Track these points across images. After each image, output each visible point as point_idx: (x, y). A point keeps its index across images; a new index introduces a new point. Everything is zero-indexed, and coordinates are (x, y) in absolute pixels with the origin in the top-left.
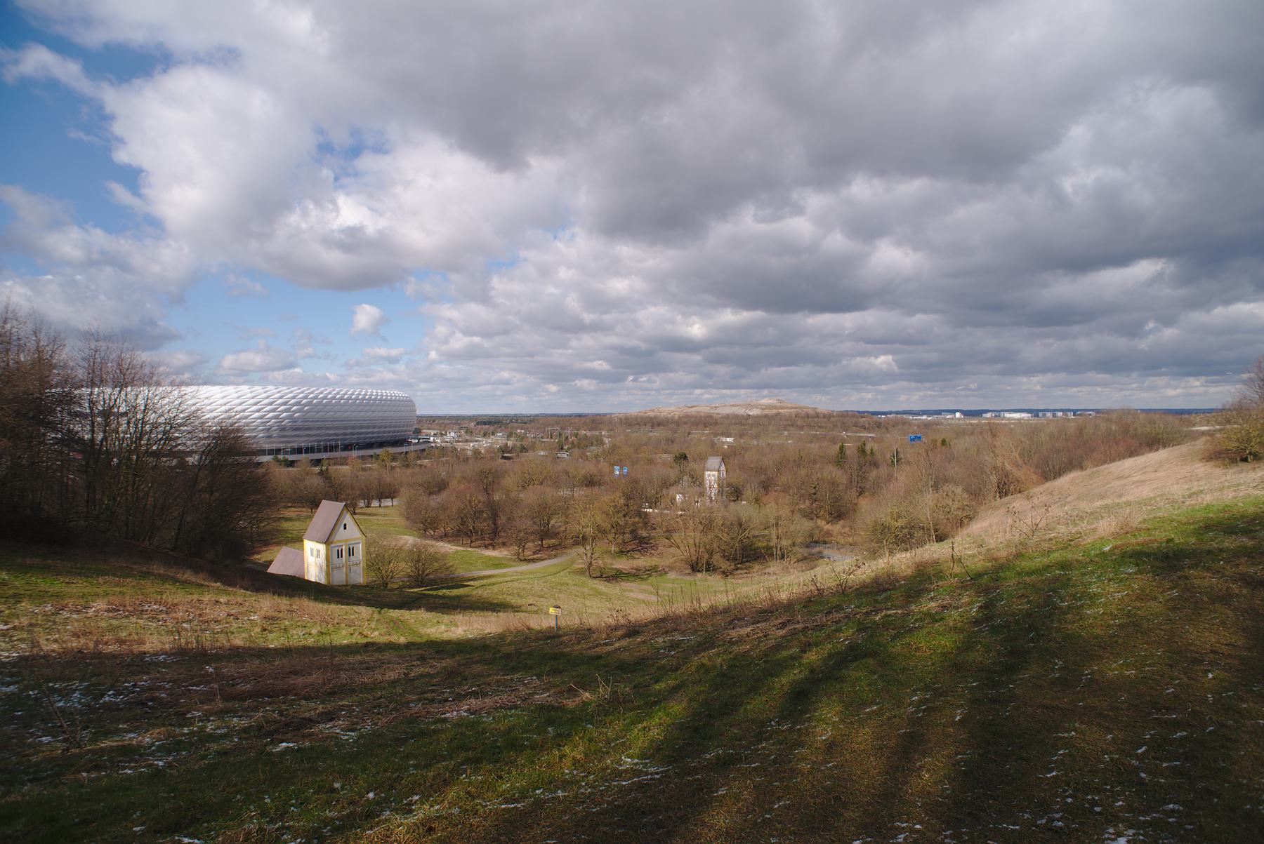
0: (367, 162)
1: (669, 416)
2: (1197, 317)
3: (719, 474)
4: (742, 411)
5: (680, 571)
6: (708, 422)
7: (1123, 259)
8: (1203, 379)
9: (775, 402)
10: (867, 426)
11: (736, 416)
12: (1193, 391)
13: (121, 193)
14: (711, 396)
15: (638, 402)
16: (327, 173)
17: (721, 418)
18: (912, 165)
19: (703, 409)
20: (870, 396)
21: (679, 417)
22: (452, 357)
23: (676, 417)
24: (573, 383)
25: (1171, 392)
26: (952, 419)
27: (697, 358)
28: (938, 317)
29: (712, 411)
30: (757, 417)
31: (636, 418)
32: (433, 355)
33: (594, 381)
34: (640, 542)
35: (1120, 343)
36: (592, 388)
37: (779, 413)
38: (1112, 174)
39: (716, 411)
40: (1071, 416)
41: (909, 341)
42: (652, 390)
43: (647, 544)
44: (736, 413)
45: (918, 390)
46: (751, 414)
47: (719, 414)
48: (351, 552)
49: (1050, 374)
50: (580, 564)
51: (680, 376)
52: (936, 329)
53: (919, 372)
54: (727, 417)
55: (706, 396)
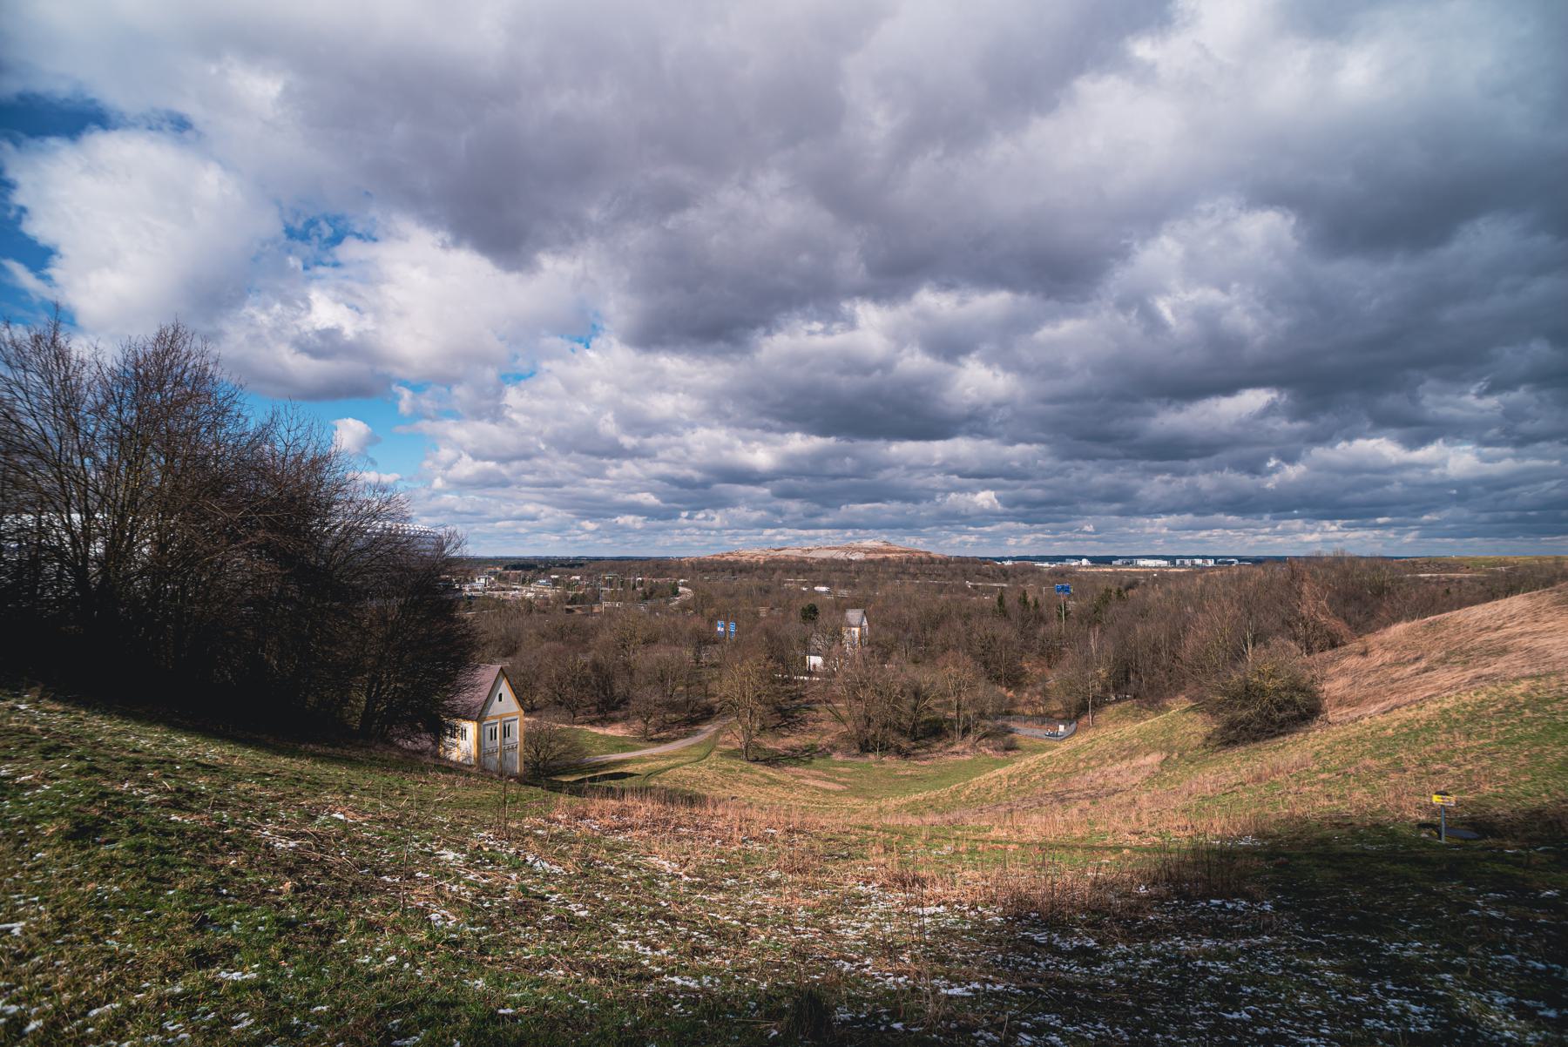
0: (351, 250)
1: (753, 560)
2: (1320, 453)
3: (861, 630)
4: (841, 555)
5: (847, 752)
6: (801, 567)
7: (1229, 388)
8: (1339, 522)
9: (881, 544)
10: (991, 573)
11: (835, 562)
12: (1329, 536)
13: (23, 276)
14: (785, 538)
15: (696, 544)
16: (293, 262)
17: (817, 563)
18: (989, 276)
19: (794, 552)
20: (973, 539)
21: (765, 562)
22: (462, 485)
23: (762, 562)
24: (614, 520)
25: (1308, 538)
26: (1079, 567)
27: (764, 491)
28: (1042, 447)
31: (712, 562)
32: (438, 483)
33: (640, 518)
34: (783, 716)
35: (1243, 481)
36: (638, 526)
37: (887, 558)
38: (1213, 296)
40: (1211, 563)
41: (1011, 474)
42: (712, 530)
43: (792, 717)
44: (835, 557)
45: (1028, 532)
46: (853, 558)
47: (813, 558)
48: (506, 732)
49: (1175, 516)
50: (738, 743)
51: (741, 512)
52: (1039, 462)
53: (1031, 512)
54: (824, 562)
55: (779, 538)
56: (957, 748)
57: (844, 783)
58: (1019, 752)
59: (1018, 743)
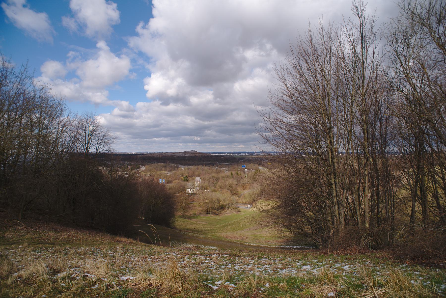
10: (224, 160)
21: (162, 157)
23: (161, 157)
29: (173, 155)
30: (189, 157)
39: (174, 155)
44: (182, 155)
46: (186, 156)
56: (227, 212)
57: (206, 222)
58: (241, 212)
59: (240, 211)
